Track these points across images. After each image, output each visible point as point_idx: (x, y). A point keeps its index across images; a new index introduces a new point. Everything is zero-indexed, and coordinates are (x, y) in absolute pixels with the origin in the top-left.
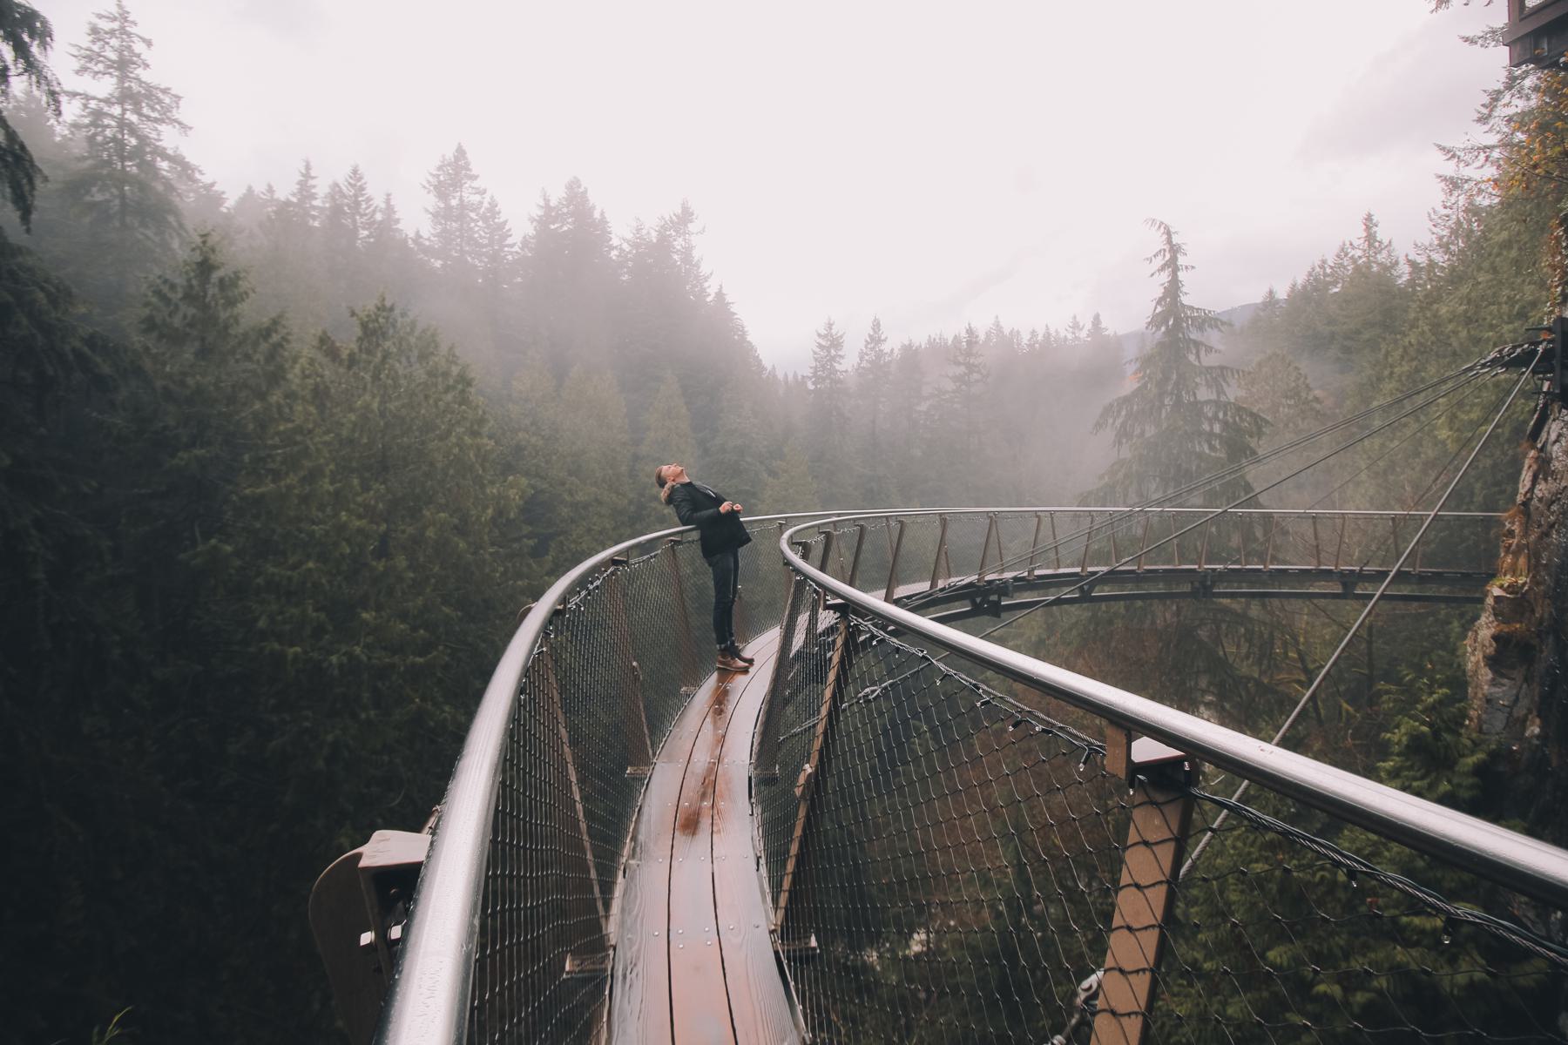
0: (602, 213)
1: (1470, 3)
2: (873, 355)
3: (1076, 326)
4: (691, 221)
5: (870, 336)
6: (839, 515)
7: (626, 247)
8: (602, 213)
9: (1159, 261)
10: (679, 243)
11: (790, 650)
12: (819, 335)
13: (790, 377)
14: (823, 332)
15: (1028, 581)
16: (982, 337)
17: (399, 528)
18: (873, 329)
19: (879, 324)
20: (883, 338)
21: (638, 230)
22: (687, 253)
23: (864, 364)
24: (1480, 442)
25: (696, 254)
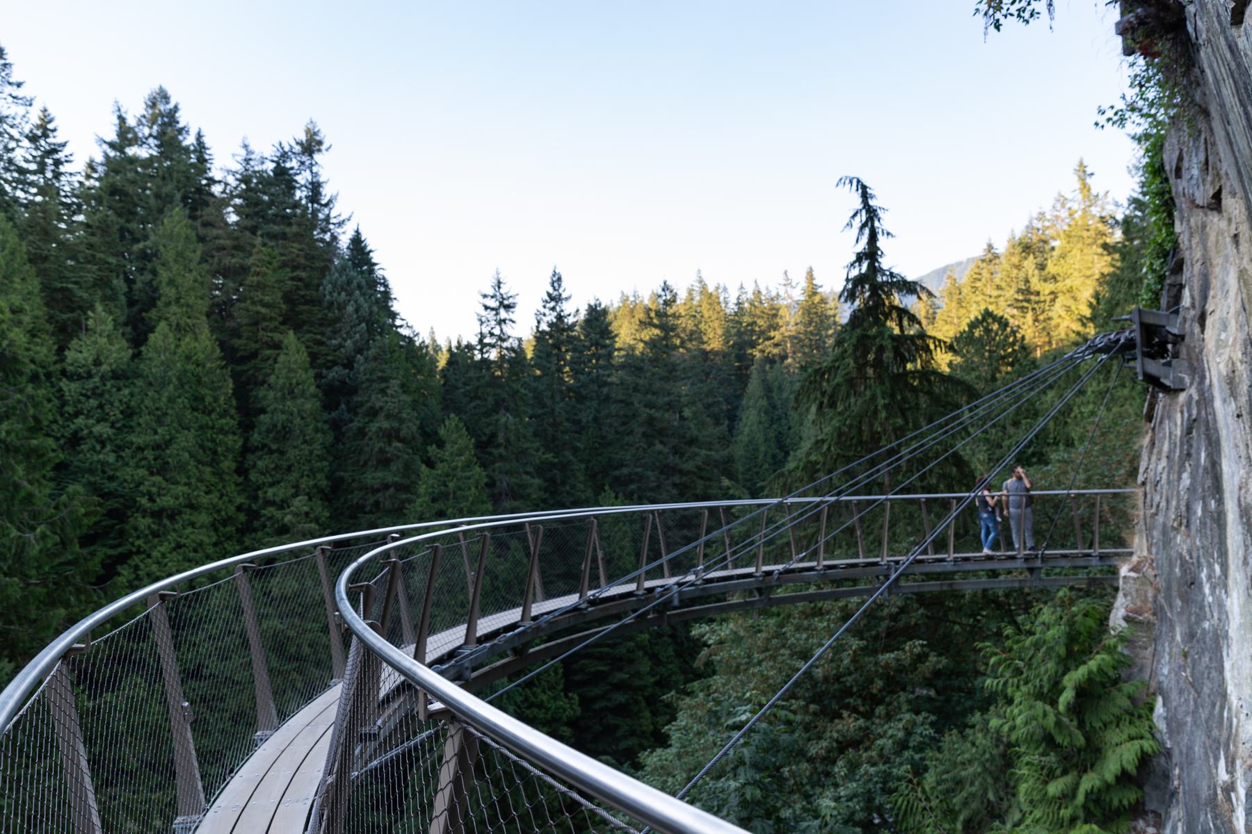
0: (199, 136)
1: (1050, 31)
2: (551, 317)
3: (1062, 201)
4: (319, 150)
5: (549, 295)
6: (469, 523)
7: (231, 180)
8: (199, 136)
9: (857, 223)
10: (303, 178)
11: (345, 698)
12: (485, 296)
13: (454, 344)
14: (491, 292)
15: (638, 595)
16: (682, 296)
17: (39, 153)
18: (553, 286)
19: (559, 279)
20: (564, 296)
21: (247, 161)
22: (315, 188)
23: (544, 327)
24: (348, 541)
25: (326, 192)
